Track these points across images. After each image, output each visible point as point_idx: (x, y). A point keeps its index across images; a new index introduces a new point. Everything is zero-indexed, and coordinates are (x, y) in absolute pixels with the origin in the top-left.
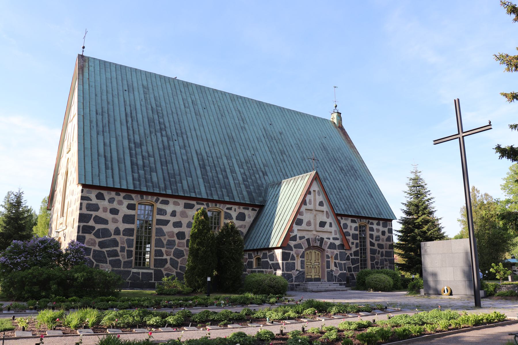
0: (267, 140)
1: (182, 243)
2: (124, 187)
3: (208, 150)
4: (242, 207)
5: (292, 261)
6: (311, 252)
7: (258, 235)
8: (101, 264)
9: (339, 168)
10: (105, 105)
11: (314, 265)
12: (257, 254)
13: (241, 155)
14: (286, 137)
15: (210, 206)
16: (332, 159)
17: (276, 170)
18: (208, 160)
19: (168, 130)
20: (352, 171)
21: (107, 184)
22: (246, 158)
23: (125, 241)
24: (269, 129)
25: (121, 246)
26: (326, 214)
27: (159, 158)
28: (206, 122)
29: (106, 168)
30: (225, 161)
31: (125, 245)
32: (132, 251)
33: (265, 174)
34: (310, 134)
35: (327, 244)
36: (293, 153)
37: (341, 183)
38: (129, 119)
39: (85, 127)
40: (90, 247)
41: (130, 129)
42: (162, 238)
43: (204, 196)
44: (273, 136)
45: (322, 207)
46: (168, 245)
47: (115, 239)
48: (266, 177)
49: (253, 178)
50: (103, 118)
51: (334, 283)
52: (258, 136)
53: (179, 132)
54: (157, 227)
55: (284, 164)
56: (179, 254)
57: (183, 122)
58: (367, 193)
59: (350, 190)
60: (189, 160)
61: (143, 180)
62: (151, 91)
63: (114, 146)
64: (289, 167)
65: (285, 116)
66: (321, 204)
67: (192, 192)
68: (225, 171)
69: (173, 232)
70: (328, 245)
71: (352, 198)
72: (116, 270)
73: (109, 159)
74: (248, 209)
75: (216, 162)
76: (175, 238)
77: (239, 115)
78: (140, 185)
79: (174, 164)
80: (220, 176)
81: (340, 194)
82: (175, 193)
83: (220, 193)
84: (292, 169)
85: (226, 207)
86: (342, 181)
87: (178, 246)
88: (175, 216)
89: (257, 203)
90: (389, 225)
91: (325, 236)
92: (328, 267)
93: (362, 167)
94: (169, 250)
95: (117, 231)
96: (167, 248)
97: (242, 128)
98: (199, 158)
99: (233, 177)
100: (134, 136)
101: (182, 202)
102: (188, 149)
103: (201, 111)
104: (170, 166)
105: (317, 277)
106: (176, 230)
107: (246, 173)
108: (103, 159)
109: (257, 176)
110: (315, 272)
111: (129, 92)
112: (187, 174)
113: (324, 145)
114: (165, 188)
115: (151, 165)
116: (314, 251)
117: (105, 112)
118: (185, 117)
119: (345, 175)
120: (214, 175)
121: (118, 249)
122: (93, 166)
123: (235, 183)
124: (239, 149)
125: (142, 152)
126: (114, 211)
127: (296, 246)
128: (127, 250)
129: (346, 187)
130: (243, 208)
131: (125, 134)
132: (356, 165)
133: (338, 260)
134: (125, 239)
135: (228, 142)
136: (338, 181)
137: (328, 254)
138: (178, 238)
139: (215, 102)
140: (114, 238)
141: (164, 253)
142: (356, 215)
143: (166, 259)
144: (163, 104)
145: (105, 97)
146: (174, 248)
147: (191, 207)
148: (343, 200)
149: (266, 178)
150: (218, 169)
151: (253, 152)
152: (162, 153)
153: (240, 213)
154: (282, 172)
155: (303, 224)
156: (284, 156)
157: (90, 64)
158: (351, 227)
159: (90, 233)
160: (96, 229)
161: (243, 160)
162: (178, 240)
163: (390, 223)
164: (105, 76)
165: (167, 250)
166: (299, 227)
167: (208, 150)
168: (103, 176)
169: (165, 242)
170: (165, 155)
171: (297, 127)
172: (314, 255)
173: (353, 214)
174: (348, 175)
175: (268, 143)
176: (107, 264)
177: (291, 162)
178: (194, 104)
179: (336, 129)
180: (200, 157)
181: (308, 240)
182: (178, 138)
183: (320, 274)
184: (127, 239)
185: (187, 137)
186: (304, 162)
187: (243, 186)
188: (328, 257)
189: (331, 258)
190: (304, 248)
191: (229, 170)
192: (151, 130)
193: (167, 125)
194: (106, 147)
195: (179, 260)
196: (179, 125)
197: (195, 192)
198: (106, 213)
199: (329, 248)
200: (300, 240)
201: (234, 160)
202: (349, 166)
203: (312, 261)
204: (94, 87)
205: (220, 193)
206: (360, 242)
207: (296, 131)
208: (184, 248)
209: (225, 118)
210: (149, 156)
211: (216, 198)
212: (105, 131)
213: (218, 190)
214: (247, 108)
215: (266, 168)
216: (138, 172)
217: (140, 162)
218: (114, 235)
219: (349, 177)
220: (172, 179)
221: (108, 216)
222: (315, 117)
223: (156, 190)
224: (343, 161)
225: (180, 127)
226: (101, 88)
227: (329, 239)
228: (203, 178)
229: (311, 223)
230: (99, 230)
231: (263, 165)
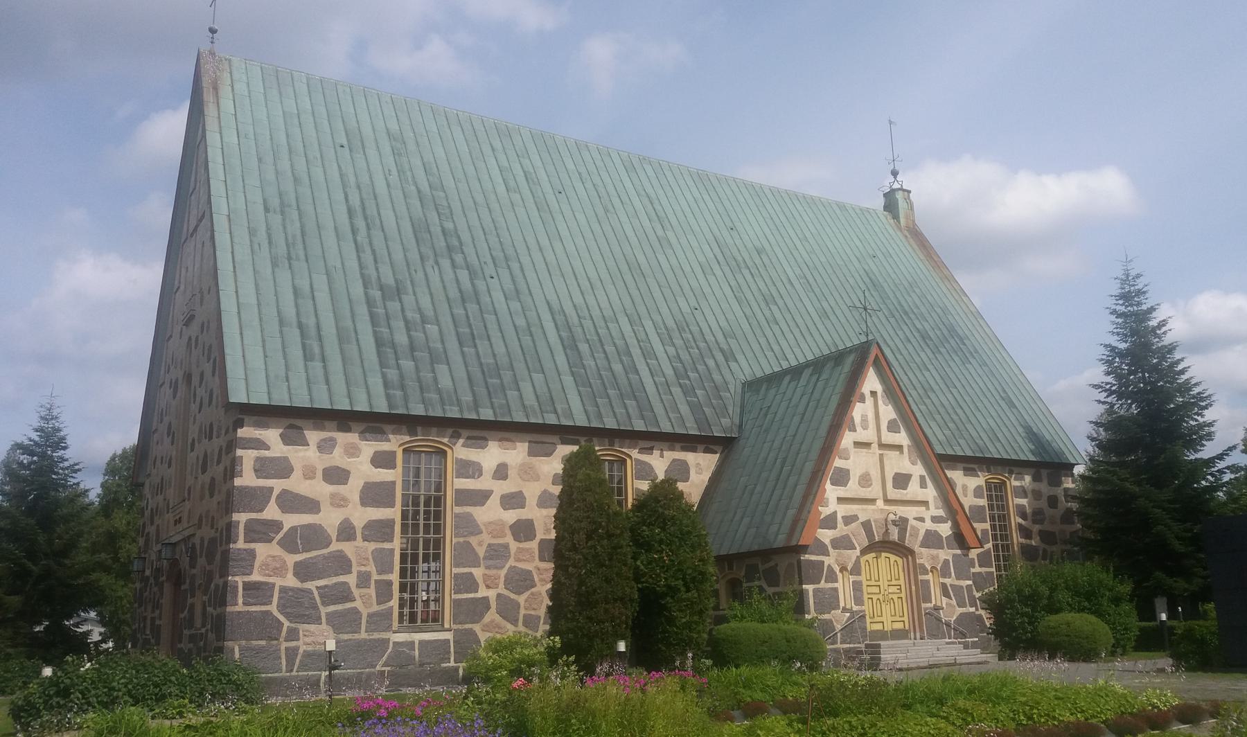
0: (727, 269)
1: (527, 550)
2: (362, 406)
3: (578, 299)
5: (830, 585)
8: (303, 627)
9: (916, 334)
10: (289, 186)
12: (731, 568)
13: (665, 310)
16: (898, 311)
17: (755, 347)
19: (469, 250)
20: (952, 341)
21: (311, 400)
22: (679, 317)
23: (370, 557)
24: (729, 241)
25: (359, 573)
27: (452, 327)
29: (307, 357)
30: (627, 328)
31: (371, 568)
32: (390, 583)
33: (729, 356)
34: (833, 250)
37: (927, 374)
38: (360, 224)
39: (236, 247)
40: (271, 580)
41: (364, 252)
42: (473, 541)
43: (581, 421)
44: (740, 259)
45: (898, 434)
46: (491, 559)
47: (341, 551)
48: (733, 365)
49: (701, 368)
50: (284, 220)
51: (948, 643)
52: (702, 259)
53: (498, 254)
54: (458, 510)
56: (520, 581)
58: (998, 397)
59: (954, 391)
60: (533, 329)
61: (412, 384)
62: (412, 146)
63: (323, 297)
64: (790, 336)
68: (629, 354)
69: (501, 523)
70: (921, 538)
71: (959, 411)
72: (347, 641)
73: (313, 332)
76: (509, 539)
78: (406, 399)
80: (618, 367)
81: (927, 401)
83: (620, 411)
86: (930, 367)
87: (518, 560)
88: (505, 477)
89: (717, 432)
91: (910, 512)
94: (493, 572)
95: (346, 531)
96: (487, 568)
98: (559, 323)
99: (650, 369)
100: (377, 269)
103: (551, 197)
104: (482, 346)
105: (899, 626)
106: (511, 516)
108: (297, 332)
109: (711, 363)
110: (893, 614)
111: (351, 151)
112: (530, 365)
113: (873, 277)
114: (476, 405)
115: (431, 345)
117: (290, 206)
121: (351, 579)
122: (268, 354)
124: (657, 294)
125: (403, 310)
126: (336, 476)
128: (376, 580)
129: (940, 381)
131: (353, 264)
132: (961, 324)
134: (370, 552)
135: (628, 278)
136: (918, 366)
139: (585, 175)
140: (340, 548)
141: (480, 581)
142: (977, 455)
143: (486, 599)
144: (449, 183)
145: (285, 164)
146: (507, 566)
148: (938, 417)
150: (610, 349)
151: (693, 303)
152: (459, 311)
153: (674, 460)
154: (773, 351)
156: (774, 308)
157: (236, 76)
158: (965, 488)
159: (270, 541)
160: (285, 529)
161: (671, 323)
164: (280, 108)
165: (487, 572)
167: (578, 299)
168: (299, 381)
169: (481, 552)
170: (468, 317)
171: (799, 232)
172: (886, 567)
173: (969, 453)
174: (942, 350)
176: (321, 624)
177: (792, 324)
178: (530, 181)
181: (867, 525)
183: (905, 618)
184: (376, 549)
186: (827, 322)
187: (676, 391)
190: (858, 548)
191: (639, 351)
192: (423, 249)
193: (465, 237)
194: (300, 301)
195: (521, 599)
197: (556, 412)
198: (313, 482)
200: (846, 525)
201: (648, 325)
202: (942, 326)
203: (880, 583)
204: (253, 138)
205: (620, 411)
206: (993, 527)
210: (424, 320)
211: (610, 424)
212: (294, 257)
215: (732, 342)
216: (398, 367)
217: (401, 338)
218: (337, 540)
219: (947, 357)
221: (318, 489)
223: (451, 410)
224: (927, 315)
226: (271, 139)
227: (922, 520)
228: (573, 374)
229: (870, 480)
230: (293, 529)
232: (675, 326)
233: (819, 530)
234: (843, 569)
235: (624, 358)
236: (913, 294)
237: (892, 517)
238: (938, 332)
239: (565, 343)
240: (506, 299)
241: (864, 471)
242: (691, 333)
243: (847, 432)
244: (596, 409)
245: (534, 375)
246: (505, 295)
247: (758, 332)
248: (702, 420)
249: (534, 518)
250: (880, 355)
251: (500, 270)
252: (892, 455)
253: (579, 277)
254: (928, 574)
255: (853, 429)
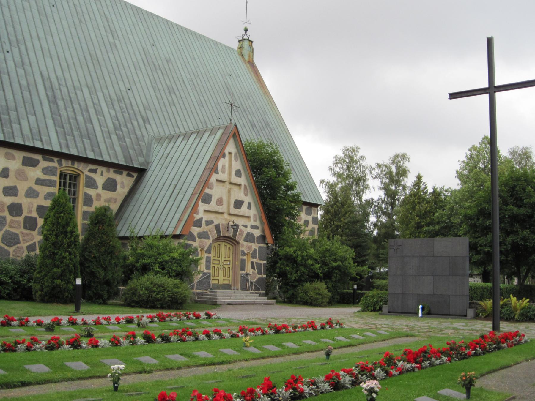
1: (17, 221)
4: (112, 170)
6: (220, 245)
7: (139, 215)
11: (222, 264)
14: (176, 68)
15: (64, 165)
18: (60, 90)
20: (266, 129)
24: (151, 52)
26: (244, 190)
28: (43, 33)
33: (146, 121)
35: (242, 234)
36: (187, 94)
43: (57, 148)
44: (156, 64)
45: (240, 178)
48: (148, 126)
49: (129, 125)
51: (251, 293)
53: (13, 39)
55: (173, 108)
57: (20, 23)
64: (181, 114)
65: (175, 35)
66: (238, 174)
67: (36, 140)
68: (88, 111)
70: (244, 236)
74: (121, 173)
75: (73, 95)
76: (6, 214)
77: (106, 23)
79: (6, 91)
80: (80, 118)
82: (9, 138)
83: (80, 145)
84: (185, 117)
85: (88, 169)
87: (11, 227)
88: (7, 176)
90: (314, 212)
91: (240, 222)
92: (243, 269)
93: (280, 124)
97: (110, 45)
98: (47, 86)
101: (20, 155)
102: (28, 68)
103: (48, 9)
105: (226, 282)
106: (9, 200)
107: (119, 118)
109: (135, 123)
113: (229, 87)
116: (224, 244)
118: (22, 15)
119: (257, 134)
120: (70, 116)
123: (102, 130)
124: (107, 79)
127: (201, 235)
130: (115, 172)
133: (256, 258)
135: (90, 65)
137: (243, 249)
138: (11, 214)
146: (4, 230)
147: (34, 164)
149: (147, 128)
150: (76, 106)
151: (128, 86)
153: (109, 178)
155: (212, 202)
156: (174, 96)
161: (114, 97)
162: (11, 217)
163: (316, 209)
166: (207, 207)
175: (150, 73)
179: (244, 64)
180: (48, 84)
181: (217, 227)
182: (11, 49)
183: (230, 279)
185: (27, 49)
186: (202, 109)
187: (114, 137)
188: (243, 254)
189: (246, 256)
191: (93, 110)
195: (11, 250)
196: (14, 27)
197: (41, 140)
199: (246, 240)
201: (100, 95)
202: (262, 121)
203: (220, 259)
205: (80, 145)
207: (189, 60)
208: (20, 230)
209: (85, 26)
211: (74, 152)
213: (78, 139)
214: (118, 14)
215: (149, 113)
220: (4, 114)
222: (216, 43)
224: (255, 113)
225: (15, 31)
227: (246, 226)
228: (53, 119)
231: (144, 107)
232: (116, 98)
233: (193, 227)
234: (202, 249)
235: (84, 113)
236: (249, 101)
237: (231, 223)
238: (260, 124)
239: (50, 99)
240: (16, 66)
241: (220, 197)
242: (125, 104)
243: (214, 174)
244: (65, 142)
245: (30, 116)
246: (15, 64)
247: (164, 109)
248: (128, 157)
249: (22, 203)
250: (236, 132)
251: (13, 48)
252: (235, 189)
253: (61, 59)
254: (245, 256)
255: (217, 172)
